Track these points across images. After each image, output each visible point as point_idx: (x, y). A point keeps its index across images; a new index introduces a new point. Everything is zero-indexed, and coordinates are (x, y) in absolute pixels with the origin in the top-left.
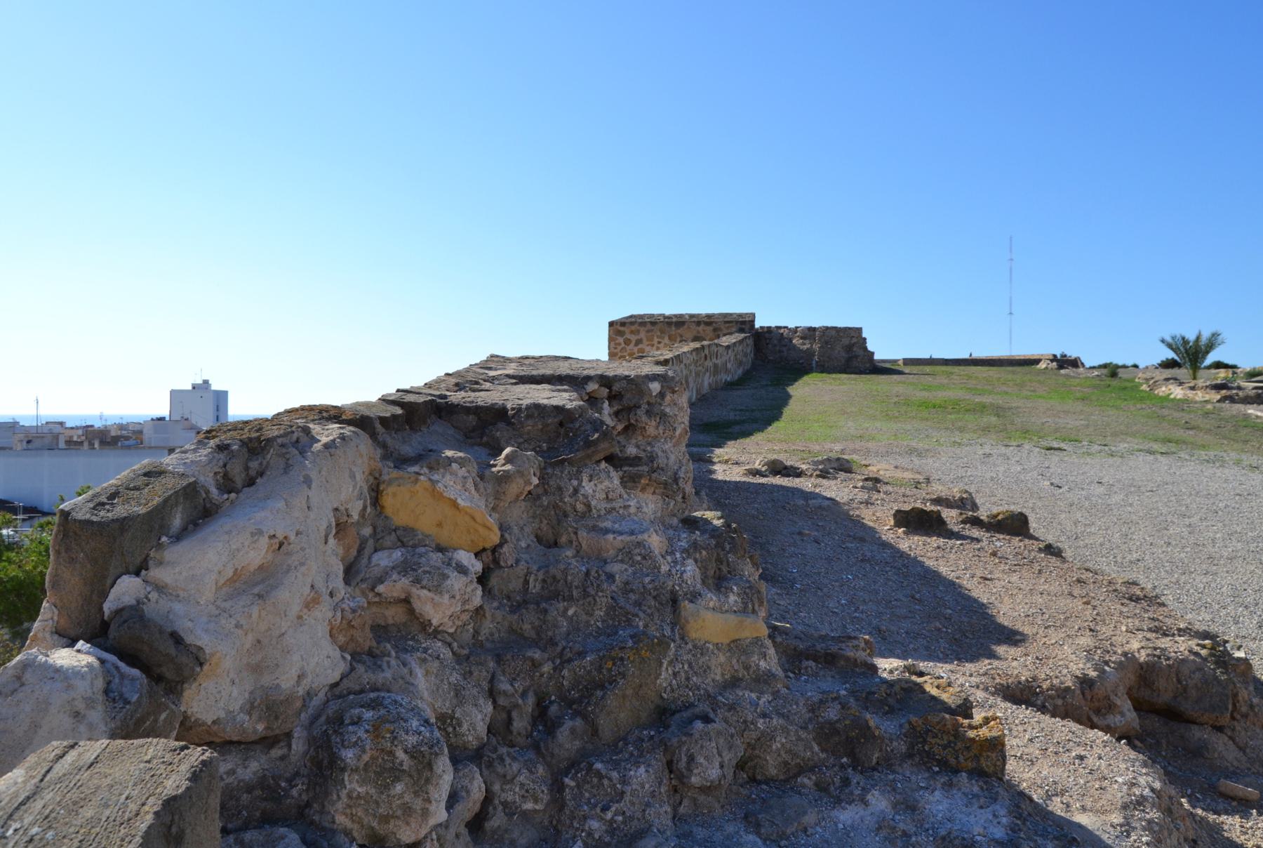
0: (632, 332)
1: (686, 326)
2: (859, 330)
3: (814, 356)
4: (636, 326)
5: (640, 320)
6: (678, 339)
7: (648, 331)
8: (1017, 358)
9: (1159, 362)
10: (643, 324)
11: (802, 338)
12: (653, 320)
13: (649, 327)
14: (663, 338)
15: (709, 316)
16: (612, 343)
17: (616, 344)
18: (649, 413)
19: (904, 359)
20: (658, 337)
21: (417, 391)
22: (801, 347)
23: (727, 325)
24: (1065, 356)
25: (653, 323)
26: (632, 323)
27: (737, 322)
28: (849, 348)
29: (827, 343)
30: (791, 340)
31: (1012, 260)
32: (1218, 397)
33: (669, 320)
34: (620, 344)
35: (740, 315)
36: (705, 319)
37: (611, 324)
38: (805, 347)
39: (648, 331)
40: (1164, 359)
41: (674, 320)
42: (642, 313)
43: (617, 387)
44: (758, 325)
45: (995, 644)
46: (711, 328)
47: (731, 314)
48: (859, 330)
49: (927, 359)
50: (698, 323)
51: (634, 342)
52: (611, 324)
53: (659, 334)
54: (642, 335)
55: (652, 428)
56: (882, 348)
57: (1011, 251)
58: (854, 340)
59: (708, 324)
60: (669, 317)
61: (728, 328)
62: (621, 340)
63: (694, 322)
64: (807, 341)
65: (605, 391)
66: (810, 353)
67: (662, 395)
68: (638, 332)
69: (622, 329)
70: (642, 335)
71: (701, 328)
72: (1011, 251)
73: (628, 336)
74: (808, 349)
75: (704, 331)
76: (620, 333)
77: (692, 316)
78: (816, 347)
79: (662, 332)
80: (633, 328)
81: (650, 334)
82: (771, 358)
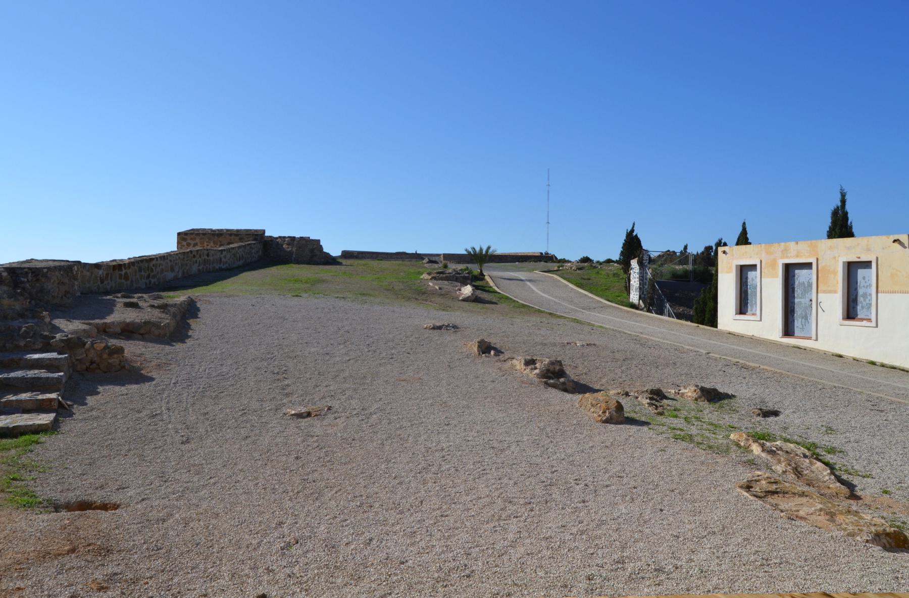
0: (191, 239)
1: (223, 236)
2: (318, 241)
3: (293, 254)
4: (194, 235)
5: (197, 232)
6: (219, 244)
7: (201, 239)
8: (513, 254)
9: (580, 259)
10: (198, 234)
11: (287, 245)
12: (204, 232)
13: (201, 236)
14: (210, 243)
15: (238, 231)
16: (180, 245)
17: (181, 246)
18: (42, 276)
19: (444, 254)
20: (207, 242)
21: (734, 333)
22: (287, 249)
23: (247, 236)
24: (548, 254)
25: (204, 234)
26: (192, 234)
27: (253, 235)
28: (312, 251)
29: (300, 247)
30: (282, 245)
31: (549, 185)
32: (430, 277)
33: (214, 233)
34: (184, 246)
35: (256, 231)
36: (235, 233)
37: (179, 234)
38: (289, 249)
39: (201, 239)
40: (585, 256)
41: (217, 232)
42: (199, 228)
43: (33, 270)
44: (267, 234)
45: (174, 342)
46: (238, 238)
47: (251, 230)
48: (318, 241)
49: (412, 254)
50: (231, 235)
51: (192, 245)
52: (179, 234)
53: (207, 240)
54: (198, 241)
55: (43, 280)
56: (333, 248)
57: (548, 179)
58: (315, 246)
59: (236, 235)
60: (214, 231)
61: (248, 238)
62: (184, 243)
63: (228, 234)
64: (290, 246)
65: (30, 271)
66: (291, 253)
67: (47, 272)
68: (195, 239)
69: (185, 237)
70: (198, 241)
71: (233, 237)
72: (548, 179)
73: (189, 241)
74: (290, 250)
75: (234, 239)
76: (185, 240)
77: (228, 230)
78: (294, 249)
79: (209, 239)
80: (192, 236)
81: (202, 240)
82: (272, 255)
